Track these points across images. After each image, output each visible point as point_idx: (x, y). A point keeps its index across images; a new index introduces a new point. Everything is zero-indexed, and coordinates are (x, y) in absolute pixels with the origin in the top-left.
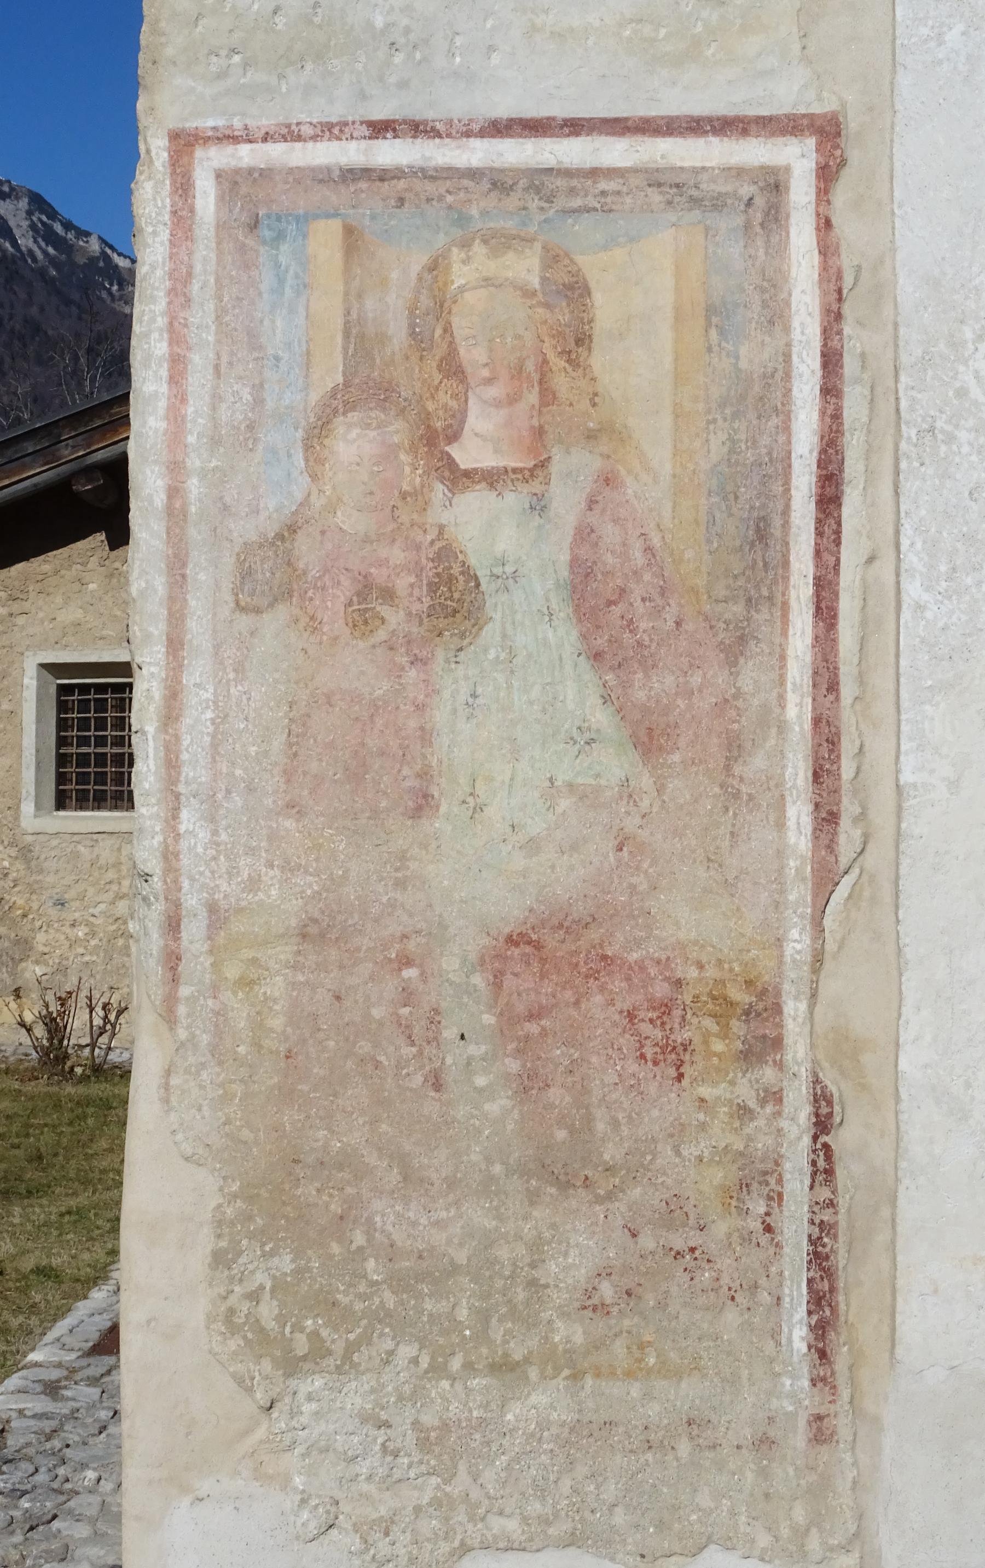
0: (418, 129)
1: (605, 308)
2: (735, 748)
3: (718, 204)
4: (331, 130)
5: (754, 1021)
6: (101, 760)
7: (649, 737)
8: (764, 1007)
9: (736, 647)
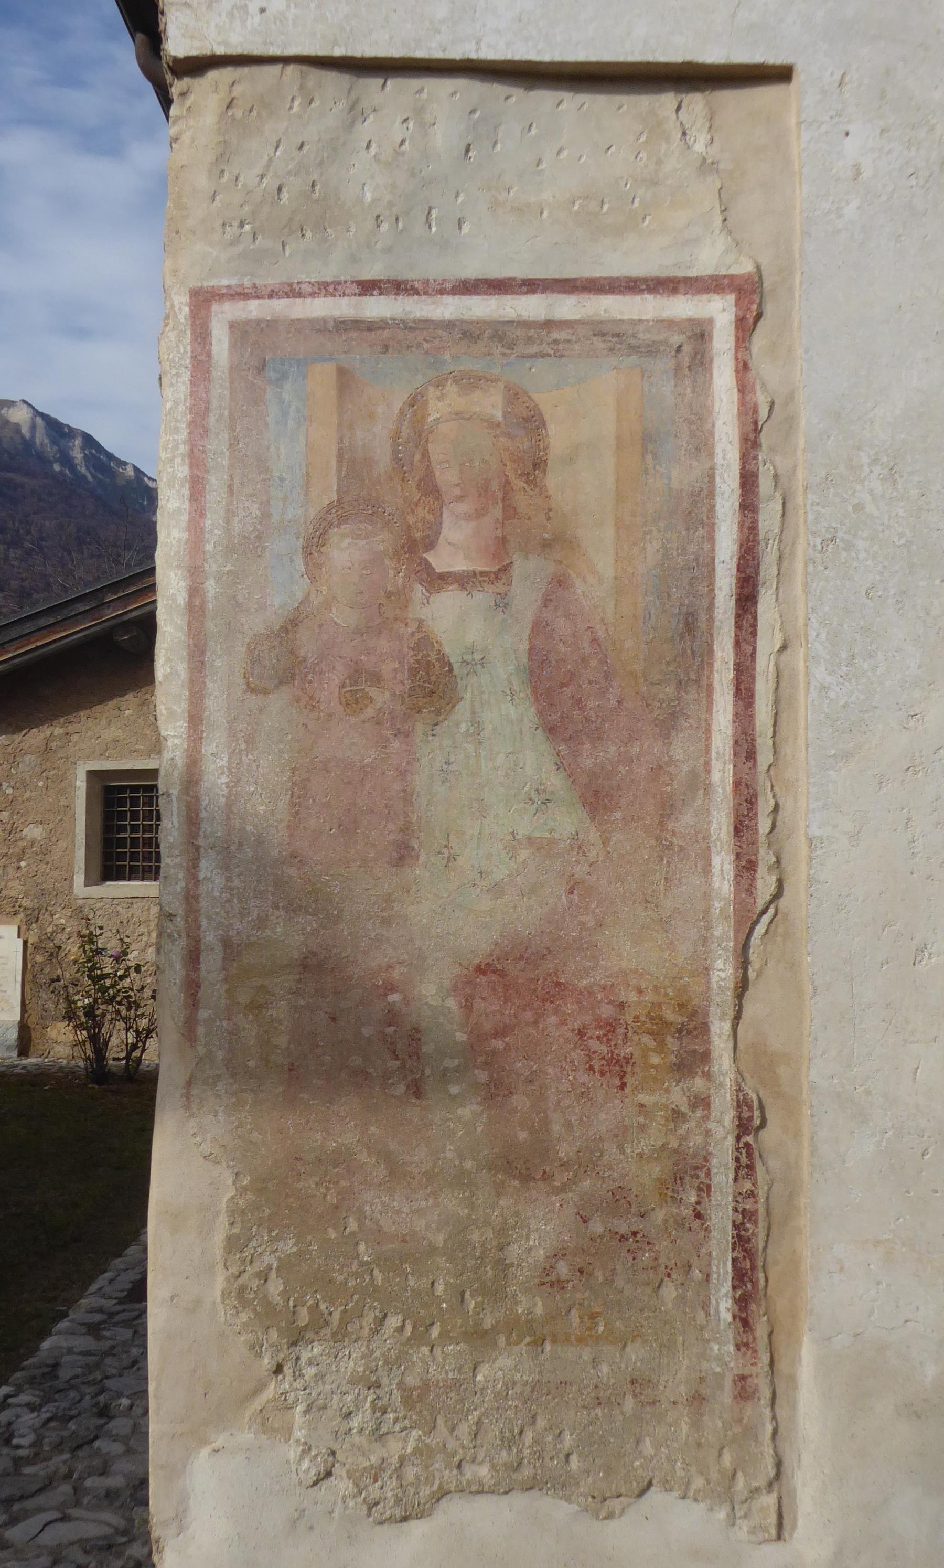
0: (399, 287)
1: (558, 437)
2: (668, 808)
3: (652, 350)
4: (327, 288)
5: (682, 1035)
7: (596, 798)
8: (695, 1026)
9: (669, 723)
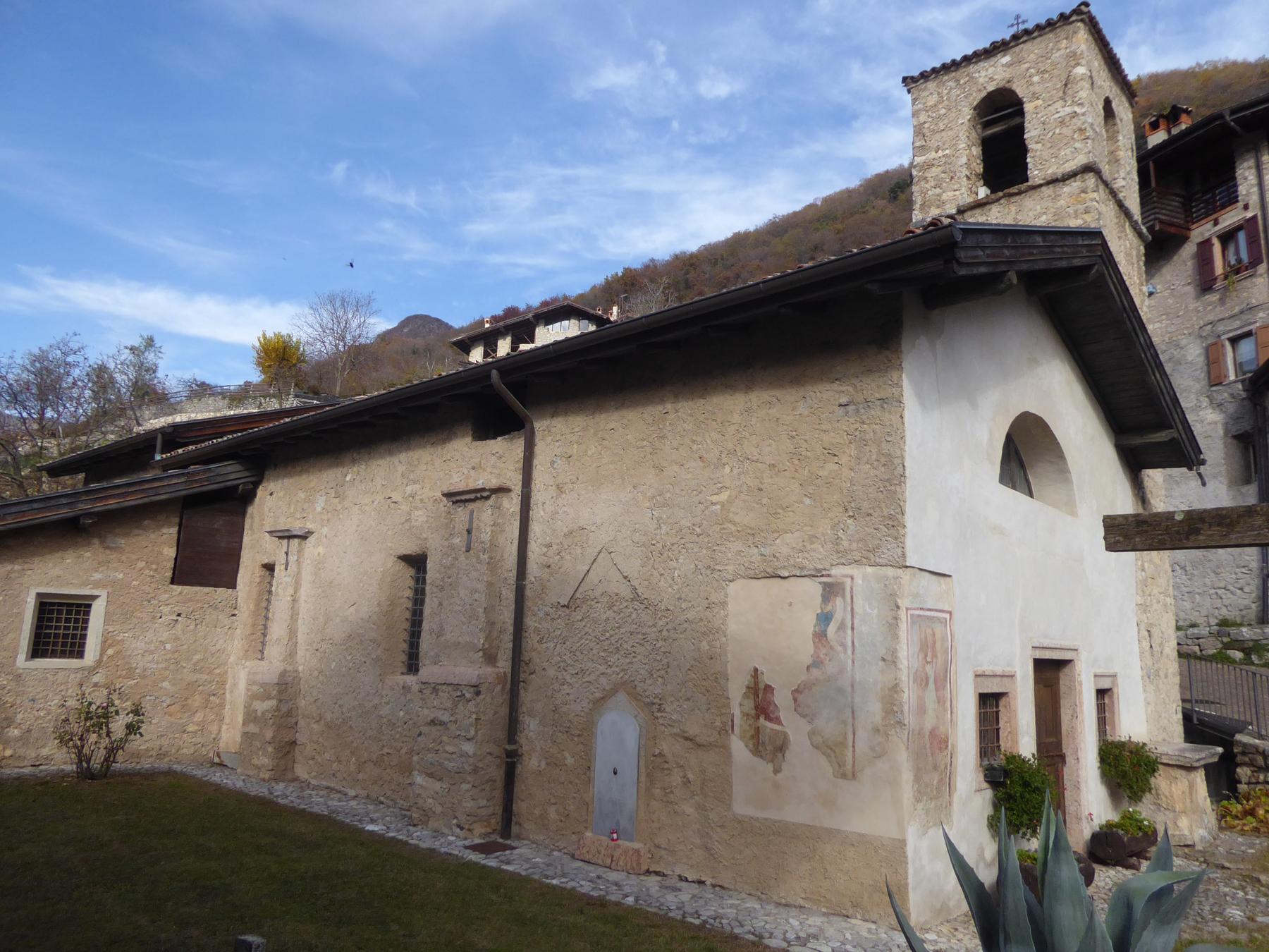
6: (74, 636)
